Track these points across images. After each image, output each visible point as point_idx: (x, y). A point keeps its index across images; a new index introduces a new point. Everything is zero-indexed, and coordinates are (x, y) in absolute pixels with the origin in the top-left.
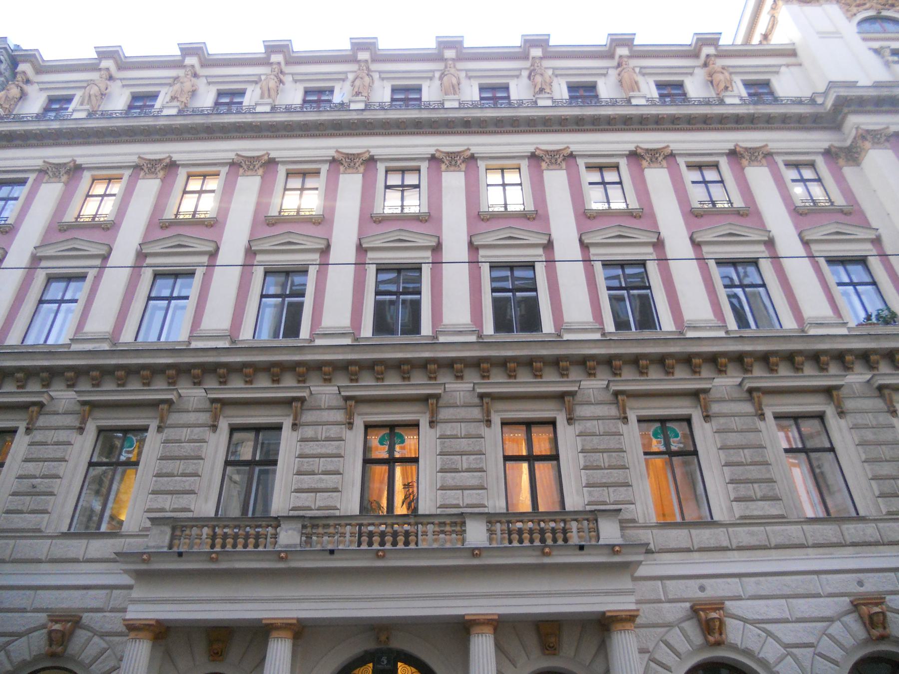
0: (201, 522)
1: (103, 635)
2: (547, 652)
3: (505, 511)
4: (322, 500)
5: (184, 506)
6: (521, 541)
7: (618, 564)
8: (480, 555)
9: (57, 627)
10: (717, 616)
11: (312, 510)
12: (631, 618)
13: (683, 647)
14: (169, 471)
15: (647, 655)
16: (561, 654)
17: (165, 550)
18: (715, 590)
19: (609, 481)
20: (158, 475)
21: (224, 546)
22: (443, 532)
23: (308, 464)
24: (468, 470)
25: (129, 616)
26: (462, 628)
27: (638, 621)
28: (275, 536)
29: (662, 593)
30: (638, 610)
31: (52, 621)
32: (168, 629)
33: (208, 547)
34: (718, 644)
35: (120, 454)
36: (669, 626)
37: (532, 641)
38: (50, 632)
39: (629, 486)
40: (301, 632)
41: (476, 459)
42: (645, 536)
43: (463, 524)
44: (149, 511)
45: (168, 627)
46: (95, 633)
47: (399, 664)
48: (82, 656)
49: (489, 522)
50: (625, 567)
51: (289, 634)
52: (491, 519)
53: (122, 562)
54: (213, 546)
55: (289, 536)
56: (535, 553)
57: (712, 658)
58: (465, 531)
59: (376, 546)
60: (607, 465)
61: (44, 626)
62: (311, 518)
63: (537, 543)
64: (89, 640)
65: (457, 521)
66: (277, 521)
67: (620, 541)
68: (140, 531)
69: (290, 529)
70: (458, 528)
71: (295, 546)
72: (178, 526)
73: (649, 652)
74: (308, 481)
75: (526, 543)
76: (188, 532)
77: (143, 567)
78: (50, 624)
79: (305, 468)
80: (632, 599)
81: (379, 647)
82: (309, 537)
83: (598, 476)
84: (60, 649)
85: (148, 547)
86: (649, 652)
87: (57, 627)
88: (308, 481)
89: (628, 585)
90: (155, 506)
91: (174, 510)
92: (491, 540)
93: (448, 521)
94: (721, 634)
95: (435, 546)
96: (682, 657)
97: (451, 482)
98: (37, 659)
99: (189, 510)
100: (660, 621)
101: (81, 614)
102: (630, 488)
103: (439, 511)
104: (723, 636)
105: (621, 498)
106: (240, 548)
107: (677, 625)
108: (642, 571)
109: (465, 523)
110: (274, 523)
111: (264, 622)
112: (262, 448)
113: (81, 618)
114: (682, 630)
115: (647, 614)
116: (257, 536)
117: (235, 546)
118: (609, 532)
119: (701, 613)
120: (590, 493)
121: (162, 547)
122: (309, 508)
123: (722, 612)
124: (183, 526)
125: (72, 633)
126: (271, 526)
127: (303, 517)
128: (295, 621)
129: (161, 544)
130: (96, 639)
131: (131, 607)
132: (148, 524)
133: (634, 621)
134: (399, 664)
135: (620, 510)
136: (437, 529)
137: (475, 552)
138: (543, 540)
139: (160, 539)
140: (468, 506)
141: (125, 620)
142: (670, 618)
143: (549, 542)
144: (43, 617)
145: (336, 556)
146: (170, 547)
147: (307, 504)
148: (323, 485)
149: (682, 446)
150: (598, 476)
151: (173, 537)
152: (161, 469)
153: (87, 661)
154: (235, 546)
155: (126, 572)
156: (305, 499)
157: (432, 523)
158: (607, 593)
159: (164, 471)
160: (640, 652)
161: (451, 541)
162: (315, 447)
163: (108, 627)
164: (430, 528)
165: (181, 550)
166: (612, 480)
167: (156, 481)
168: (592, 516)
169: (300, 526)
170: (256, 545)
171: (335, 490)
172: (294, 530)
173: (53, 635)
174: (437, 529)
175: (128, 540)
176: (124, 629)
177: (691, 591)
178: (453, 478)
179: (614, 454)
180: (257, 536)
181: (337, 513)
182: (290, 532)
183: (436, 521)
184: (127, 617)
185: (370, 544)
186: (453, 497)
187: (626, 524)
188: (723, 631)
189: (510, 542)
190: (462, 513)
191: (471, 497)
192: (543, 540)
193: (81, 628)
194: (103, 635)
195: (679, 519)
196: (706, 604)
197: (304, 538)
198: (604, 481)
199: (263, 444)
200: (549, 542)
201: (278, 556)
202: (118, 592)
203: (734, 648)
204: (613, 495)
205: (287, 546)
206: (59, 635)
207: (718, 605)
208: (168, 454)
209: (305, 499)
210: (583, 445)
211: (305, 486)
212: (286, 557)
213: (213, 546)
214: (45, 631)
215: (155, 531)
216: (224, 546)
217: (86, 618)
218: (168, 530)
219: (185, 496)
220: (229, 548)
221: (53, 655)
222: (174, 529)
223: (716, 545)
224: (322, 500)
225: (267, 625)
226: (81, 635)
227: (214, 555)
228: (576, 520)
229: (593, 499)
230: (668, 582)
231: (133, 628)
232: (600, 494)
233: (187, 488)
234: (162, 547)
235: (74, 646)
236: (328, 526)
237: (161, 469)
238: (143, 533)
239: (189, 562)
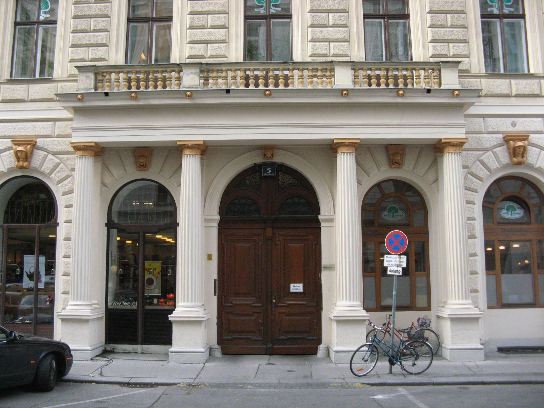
0: (116, 69)
1: (55, 154)
2: (393, 166)
3: (364, 60)
4: (212, 49)
5: (99, 56)
6: (378, 85)
7: (456, 104)
8: (348, 95)
9: (20, 148)
10: (523, 145)
11: (205, 58)
12: (458, 145)
13: (494, 164)
14: (83, 27)
15: (466, 170)
16: (404, 168)
17: (93, 91)
18: (523, 125)
19: (450, 38)
20: (74, 32)
21: (138, 87)
22: (315, 76)
23: (199, 20)
24: (334, 26)
25: (73, 140)
26: (331, 149)
27: (465, 146)
28: (179, 79)
29: (483, 127)
30: (467, 139)
31: (16, 145)
32: (103, 148)
33: (126, 88)
34: (519, 164)
35: (39, 14)
36: (486, 150)
37: (382, 158)
38: (16, 153)
39: (467, 43)
40: (205, 150)
41: (341, 16)
42: (474, 83)
43: (332, 70)
44: (72, 61)
45: (103, 148)
46: (49, 152)
47: (280, 173)
48: (42, 170)
49: (353, 69)
50: (459, 108)
51: (199, 152)
52: (355, 66)
53: (62, 101)
54: (130, 88)
55: (190, 79)
56: (391, 94)
57: (510, 173)
58: (334, 75)
59: (261, 87)
60: (449, 24)
61: (10, 148)
62: (207, 64)
63: (391, 86)
64: (45, 157)
65: (327, 68)
66: (179, 67)
67: (458, 87)
68: (69, 77)
69: (191, 73)
70: (328, 74)
71: (196, 87)
72: (100, 72)
73: (468, 168)
74: (199, 34)
75: (383, 86)
76: (108, 77)
77: (79, 104)
78: (14, 147)
79: (197, 23)
80: (463, 130)
81: (263, 161)
82: (207, 79)
83: (441, 33)
84: (25, 164)
85: (78, 89)
86: (468, 168)
87: (20, 148)
88: (199, 34)
89: (462, 121)
90: (77, 57)
91: (93, 60)
92: (354, 83)
93: (320, 68)
94: (523, 157)
95: (309, 87)
96: (492, 172)
97: (320, 36)
98: (10, 170)
99: (104, 60)
100: (479, 147)
101: (35, 140)
102: (466, 44)
103: (310, 60)
104: (525, 158)
105: (459, 52)
106: (151, 89)
107: (491, 150)
108: (472, 111)
109: (334, 69)
110: (177, 69)
111: (178, 143)
112: (156, 6)
113: (36, 142)
114: (495, 154)
115: (472, 141)
116: (164, 79)
117: (147, 87)
118: (450, 80)
119: (511, 142)
120: (434, 48)
121: (90, 89)
122: (203, 57)
123: (526, 142)
124: (103, 73)
125: (32, 153)
126: (174, 71)
127: (201, 64)
128: (202, 143)
129: (89, 87)
130: (50, 156)
131: (74, 134)
132: (76, 71)
133: (462, 146)
134: (280, 173)
135: (460, 62)
136: (311, 74)
137: (343, 92)
138: (396, 84)
139: (86, 83)
140: (335, 56)
141: (71, 143)
142: (487, 145)
143: (401, 86)
144: (8, 143)
145: (231, 94)
146: (96, 88)
147: (200, 53)
148: (212, 38)
149: (512, 10)
150: (441, 33)
151: (96, 81)
152: (76, 26)
153: (48, 172)
154: (147, 87)
155: (65, 108)
156: (199, 50)
157: (307, 69)
158: (444, 126)
159: (79, 28)
160: (463, 168)
161: (322, 83)
162: (204, 5)
163: (58, 149)
164: (306, 73)
165: (106, 91)
166: (453, 37)
167: (74, 37)
168: (435, 67)
169: (198, 70)
170: (164, 87)
171: (223, 42)
172: (194, 74)
173: (19, 154)
174: (311, 73)
175: (60, 84)
176: (72, 150)
177: (505, 125)
178: (322, 32)
179: (456, 15)
180: (164, 79)
181: (225, 60)
182: (191, 76)
183: (310, 68)
184: (73, 141)
185: (257, 85)
186: (321, 48)
187: (464, 74)
188: (525, 155)
189: (370, 85)
190: (332, 61)
191: (335, 48)
192: (396, 84)
193: (36, 149)
194: (55, 154)
195: (502, 72)
196: (515, 136)
197: (202, 81)
198: (446, 38)
199: (156, 3)
200: (401, 86)
201: (183, 94)
202: (60, 123)
203: (531, 167)
204: (453, 49)
205: (190, 87)
206: (24, 155)
207: (524, 137)
208: (79, 13)
209: (199, 50)
210: (431, 7)
211: (198, 38)
212: (191, 96)
213: (130, 88)
214: (12, 151)
215: (82, 77)
216: (138, 87)
217: (40, 142)
218: (92, 76)
219: (99, 48)
220: (142, 89)
221: (22, 168)
222: (96, 75)
223: (530, 93)
224: (212, 49)
225: (182, 145)
226: (39, 155)
227: (133, 95)
228: (424, 69)
229: (436, 53)
230: (488, 119)
231: (78, 148)
232: (441, 48)
233: (100, 41)
234: (90, 89)
235: (36, 162)
236: (222, 71)
237: (76, 26)
238: (71, 78)
239: (113, 100)
